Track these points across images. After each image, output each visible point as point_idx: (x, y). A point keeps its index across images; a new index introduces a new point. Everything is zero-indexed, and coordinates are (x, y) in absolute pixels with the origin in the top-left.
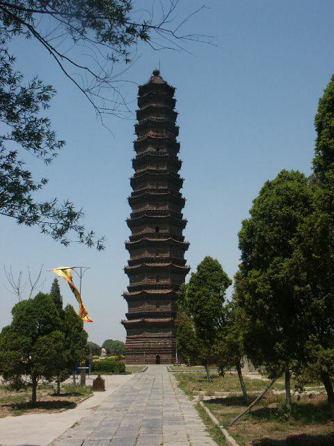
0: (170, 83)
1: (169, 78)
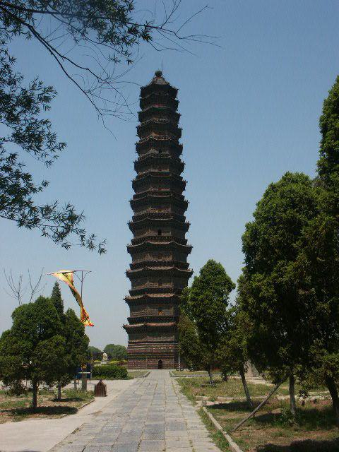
0: (173, 84)
1: (171, 79)
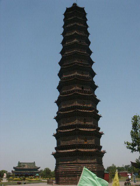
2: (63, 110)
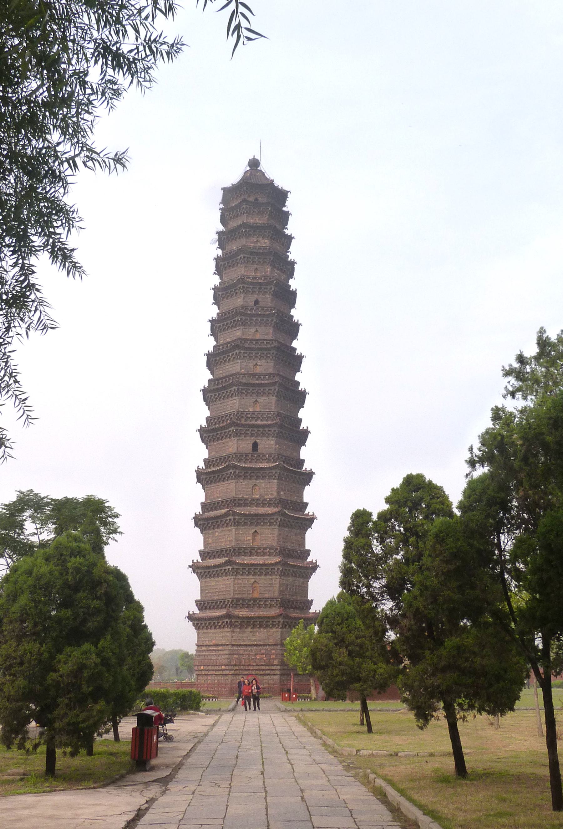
0: (280, 183)
1: (276, 173)
2: (207, 509)
